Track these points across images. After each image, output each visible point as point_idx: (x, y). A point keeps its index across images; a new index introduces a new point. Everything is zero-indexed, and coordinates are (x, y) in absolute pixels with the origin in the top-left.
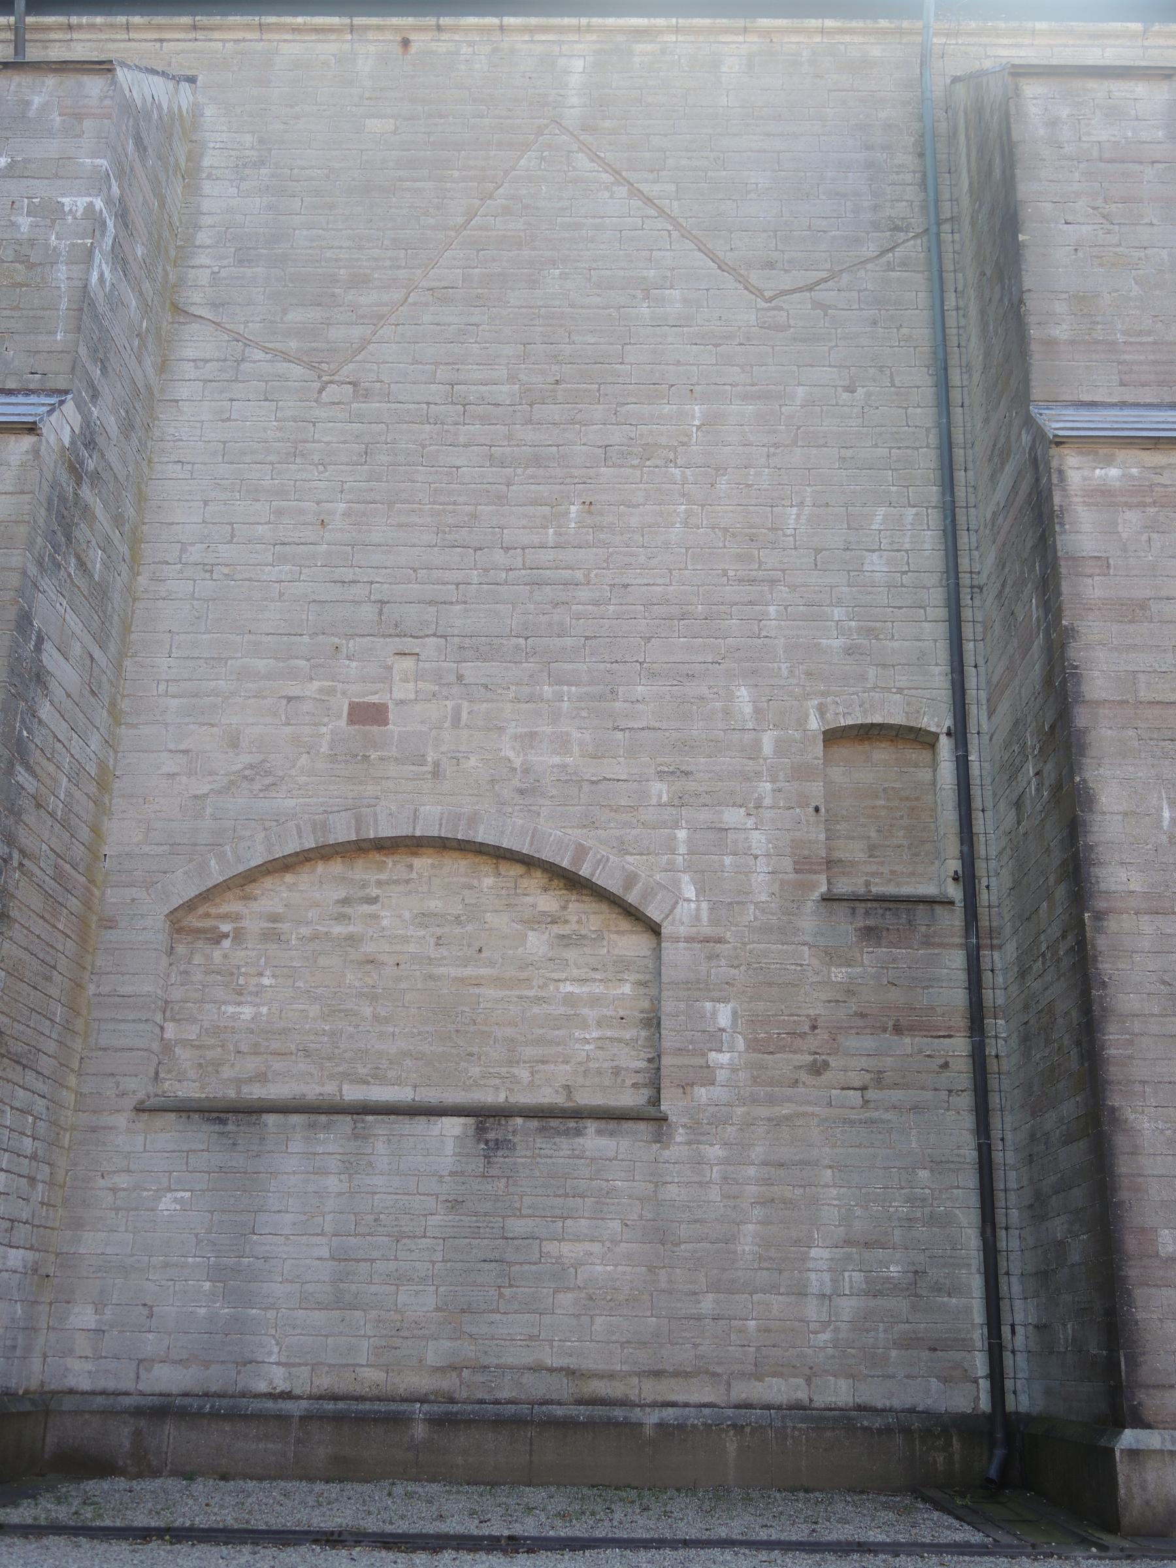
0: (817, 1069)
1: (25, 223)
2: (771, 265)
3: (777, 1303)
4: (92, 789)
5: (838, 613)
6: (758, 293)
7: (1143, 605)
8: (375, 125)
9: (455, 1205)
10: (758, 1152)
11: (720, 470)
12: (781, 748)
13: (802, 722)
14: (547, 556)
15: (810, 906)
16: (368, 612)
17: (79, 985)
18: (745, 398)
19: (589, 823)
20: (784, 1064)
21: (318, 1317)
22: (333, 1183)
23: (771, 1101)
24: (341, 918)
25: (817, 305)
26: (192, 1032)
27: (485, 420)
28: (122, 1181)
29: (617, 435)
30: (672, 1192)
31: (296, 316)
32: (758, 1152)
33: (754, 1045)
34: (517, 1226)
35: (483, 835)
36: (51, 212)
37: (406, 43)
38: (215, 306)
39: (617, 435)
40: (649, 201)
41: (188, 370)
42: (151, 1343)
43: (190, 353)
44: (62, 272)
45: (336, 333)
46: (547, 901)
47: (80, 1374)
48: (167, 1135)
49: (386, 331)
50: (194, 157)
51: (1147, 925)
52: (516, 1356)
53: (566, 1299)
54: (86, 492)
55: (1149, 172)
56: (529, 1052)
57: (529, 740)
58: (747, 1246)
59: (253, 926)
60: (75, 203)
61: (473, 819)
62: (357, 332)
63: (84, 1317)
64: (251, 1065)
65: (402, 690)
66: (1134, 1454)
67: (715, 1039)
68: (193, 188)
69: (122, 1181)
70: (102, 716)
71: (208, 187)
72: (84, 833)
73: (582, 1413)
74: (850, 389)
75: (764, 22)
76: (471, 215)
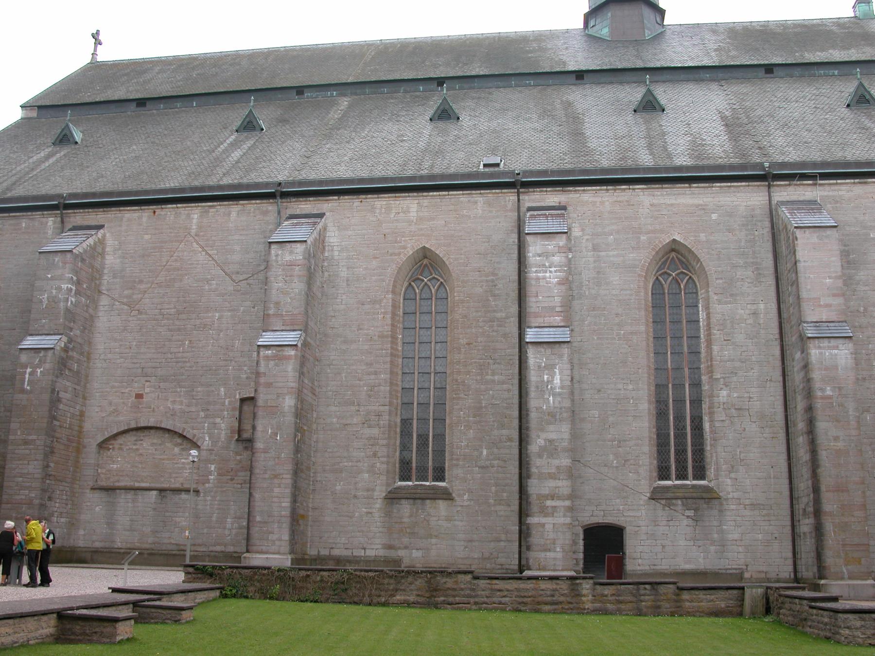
0: (232, 480)
1: (54, 291)
2: (238, 273)
3: (220, 531)
4: (78, 418)
5: (245, 368)
6: (234, 281)
7: (271, 384)
8: (147, 237)
9: (154, 509)
10: (218, 498)
11: (221, 331)
12: (230, 403)
13: (235, 396)
14: (180, 355)
15: (233, 442)
16: (140, 370)
17: (78, 462)
18: (229, 311)
19: (186, 423)
20: (225, 478)
21: (127, 533)
22: (130, 505)
23: (221, 487)
24: (135, 444)
25: (248, 284)
26: (104, 471)
27: (168, 319)
28: (89, 504)
29: (198, 322)
30: (199, 507)
31: (126, 292)
32: (218, 498)
33: (219, 474)
34: (167, 514)
35: (163, 426)
36: (59, 289)
37: (154, 212)
38: (108, 290)
39: (198, 322)
40: (210, 256)
41: (101, 308)
42: (95, 538)
43: (102, 304)
44: (62, 304)
45: (134, 297)
46: (179, 441)
47: (81, 543)
48: (97, 495)
49: (146, 295)
50: (104, 249)
51: (263, 455)
52: (166, 541)
53: (177, 529)
54: (70, 353)
55: (297, 268)
56: (174, 475)
57: (174, 402)
58: (214, 519)
59: (117, 446)
60: (64, 286)
61: (161, 422)
62: (140, 296)
63: (81, 532)
64: (116, 478)
65: (147, 390)
66: (245, 557)
67: (210, 473)
68: (103, 258)
69: (89, 504)
70: (80, 400)
71: (107, 257)
72: (77, 428)
73: (178, 553)
74: (254, 307)
75: (241, 202)
76: (167, 262)
